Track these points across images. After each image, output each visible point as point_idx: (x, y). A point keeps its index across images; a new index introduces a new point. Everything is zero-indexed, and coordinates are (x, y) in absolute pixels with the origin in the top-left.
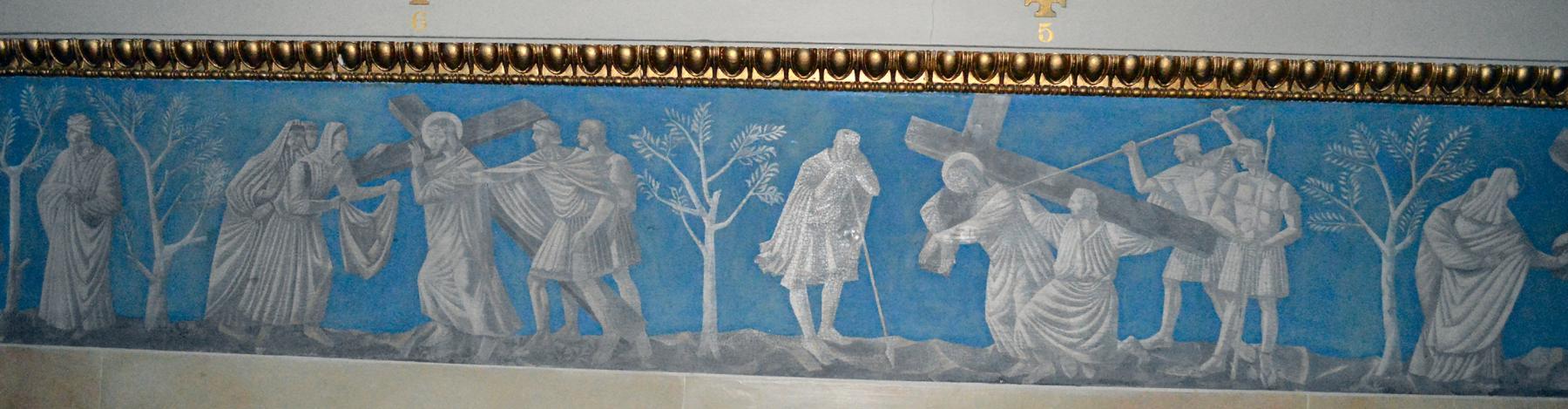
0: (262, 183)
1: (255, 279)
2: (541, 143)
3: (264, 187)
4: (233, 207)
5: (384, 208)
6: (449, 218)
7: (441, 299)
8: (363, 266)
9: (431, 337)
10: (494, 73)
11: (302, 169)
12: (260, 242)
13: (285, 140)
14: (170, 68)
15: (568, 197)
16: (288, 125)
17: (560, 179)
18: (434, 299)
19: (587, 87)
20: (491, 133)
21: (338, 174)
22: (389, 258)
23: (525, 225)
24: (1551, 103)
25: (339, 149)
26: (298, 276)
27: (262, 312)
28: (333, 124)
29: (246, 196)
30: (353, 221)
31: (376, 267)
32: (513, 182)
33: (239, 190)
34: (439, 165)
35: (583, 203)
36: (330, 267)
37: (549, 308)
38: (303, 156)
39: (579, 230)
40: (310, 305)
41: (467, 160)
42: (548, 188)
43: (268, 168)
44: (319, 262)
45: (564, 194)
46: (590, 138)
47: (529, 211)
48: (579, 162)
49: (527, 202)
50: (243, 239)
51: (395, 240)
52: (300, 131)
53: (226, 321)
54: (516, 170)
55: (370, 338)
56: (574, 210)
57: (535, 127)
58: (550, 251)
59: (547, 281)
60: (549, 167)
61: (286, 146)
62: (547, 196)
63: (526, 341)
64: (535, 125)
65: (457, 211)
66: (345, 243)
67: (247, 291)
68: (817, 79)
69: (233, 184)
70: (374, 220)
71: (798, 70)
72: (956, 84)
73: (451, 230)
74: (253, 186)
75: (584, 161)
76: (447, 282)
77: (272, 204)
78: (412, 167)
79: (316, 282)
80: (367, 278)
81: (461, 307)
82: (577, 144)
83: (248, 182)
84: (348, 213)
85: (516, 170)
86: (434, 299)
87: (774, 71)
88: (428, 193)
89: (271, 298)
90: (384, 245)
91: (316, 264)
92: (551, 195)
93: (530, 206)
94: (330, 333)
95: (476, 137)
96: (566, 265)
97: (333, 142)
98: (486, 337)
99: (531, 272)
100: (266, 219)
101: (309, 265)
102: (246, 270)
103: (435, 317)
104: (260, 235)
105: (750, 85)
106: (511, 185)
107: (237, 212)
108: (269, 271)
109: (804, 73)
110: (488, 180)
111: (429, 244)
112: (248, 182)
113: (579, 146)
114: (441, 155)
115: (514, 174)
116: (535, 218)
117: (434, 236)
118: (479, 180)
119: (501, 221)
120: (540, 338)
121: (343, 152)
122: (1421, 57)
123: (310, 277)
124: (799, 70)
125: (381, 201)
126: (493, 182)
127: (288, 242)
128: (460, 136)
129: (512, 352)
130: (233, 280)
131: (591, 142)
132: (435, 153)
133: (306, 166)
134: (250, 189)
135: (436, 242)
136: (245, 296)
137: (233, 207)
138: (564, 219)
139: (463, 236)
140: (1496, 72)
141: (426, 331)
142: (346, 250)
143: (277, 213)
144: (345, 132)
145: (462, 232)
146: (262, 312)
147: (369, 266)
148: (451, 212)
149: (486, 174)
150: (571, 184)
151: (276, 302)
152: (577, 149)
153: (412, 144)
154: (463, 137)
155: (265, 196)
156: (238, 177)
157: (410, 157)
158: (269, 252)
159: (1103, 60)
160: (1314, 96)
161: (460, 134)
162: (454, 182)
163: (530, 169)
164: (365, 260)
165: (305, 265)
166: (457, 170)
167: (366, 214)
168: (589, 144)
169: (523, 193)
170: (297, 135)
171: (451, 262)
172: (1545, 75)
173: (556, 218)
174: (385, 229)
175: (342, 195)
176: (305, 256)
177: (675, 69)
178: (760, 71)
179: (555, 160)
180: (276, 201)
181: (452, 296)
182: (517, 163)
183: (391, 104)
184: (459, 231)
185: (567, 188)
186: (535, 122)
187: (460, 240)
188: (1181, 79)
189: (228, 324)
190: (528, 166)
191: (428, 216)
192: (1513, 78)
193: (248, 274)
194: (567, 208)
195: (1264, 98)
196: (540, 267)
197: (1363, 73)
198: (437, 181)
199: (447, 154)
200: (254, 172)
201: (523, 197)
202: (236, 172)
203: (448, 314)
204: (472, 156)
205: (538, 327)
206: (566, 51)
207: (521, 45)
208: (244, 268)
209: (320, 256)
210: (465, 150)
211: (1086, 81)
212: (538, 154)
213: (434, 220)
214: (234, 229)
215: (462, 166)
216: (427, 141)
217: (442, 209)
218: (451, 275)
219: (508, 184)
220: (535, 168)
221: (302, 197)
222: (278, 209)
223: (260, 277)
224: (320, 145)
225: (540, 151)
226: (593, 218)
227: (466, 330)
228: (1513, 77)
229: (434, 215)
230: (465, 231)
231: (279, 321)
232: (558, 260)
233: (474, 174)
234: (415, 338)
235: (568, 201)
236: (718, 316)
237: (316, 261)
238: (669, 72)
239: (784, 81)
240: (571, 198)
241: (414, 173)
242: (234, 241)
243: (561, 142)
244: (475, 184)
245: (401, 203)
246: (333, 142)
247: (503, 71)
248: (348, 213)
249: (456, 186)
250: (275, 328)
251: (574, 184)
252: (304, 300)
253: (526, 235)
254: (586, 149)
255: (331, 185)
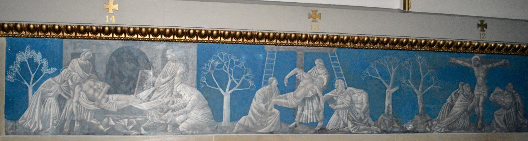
10: (59, 35)
14: (11, 33)
19: (130, 41)
24: (403, 49)
68: (242, 41)
71: (178, 36)
72: (251, 42)
87: (169, 36)
105: (243, 43)
109: (180, 37)
122: (28, 22)
124: (178, 36)
136: (38, 105)
140: (388, 40)
159: (241, 33)
160: (326, 46)
172: (362, 39)
177: (219, 37)
178: (165, 36)
188: (75, 32)
192: (402, 42)
195: (429, 51)
197: (209, 34)
206: (48, 26)
207: (56, 25)
211: (236, 40)
228: (412, 42)
238: (109, 35)
239: (124, 37)
247: (359, 45)
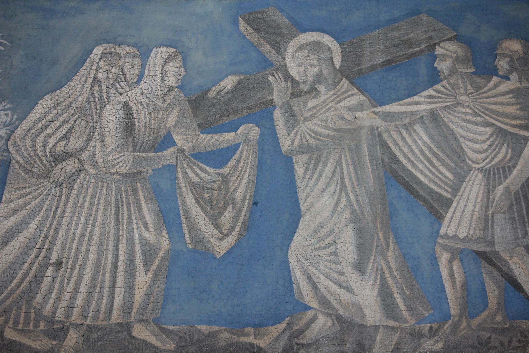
0: (63, 131)
1: (59, 264)
2: (446, 72)
3: (66, 137)
4: (20, 165)
5: (238, 161)
6: (328, 172)
7: (322, 280)
8: (212, 240)
9: (307, 332)
11: (121, 112)
12: (64, 212)
13: (93, 72)
15: (485, 141)
16: (98, 51)
17: (473, 119)
18: (310, 278)
20: (379, 59)
21: (171, 121)
22: (247, 228)
23: (430, 180)
25: (171, 84)
26: (121, 258)
27: (70, 308)
28: (161, 50)
29: (39, 150)
30: (195, 179)
31: (231, 240)
32: (411, 124)
33: (28, 141)
34: (311, 104)
35: (504, 149)
36: (165, 243)
37: (465, 285)
38: (121, 94)
39: (500, 183)
40: (139, 295)
41: (349, 97)
42: (458, 131)
43: (71, 111)
44: (150, 237)
45: (479, 138)
46: (511, 61)
47: (435, 161)
48: (497, 96)
49: (430, 149)
50: (37, 210)
51: (255, 204)
52: (114, 59)
53: (16, 323)
54: (415, 108)
55: (226, 335)
56: (493, 158)
57: (439, 50)
58: (464, 211)
59: (462, 251)
60: (458, 104)
61: (96, 80)
62: (457, 140)
63: (437, 331)
64: (437, 48)
65: (339, 163)
66: (184, 202)
67: (47, 281)
69: (19, 132)
70: (225, 179)
73: (331, 189)
74: (49, 136)
75: (504, 94)
76: (328, 258)
77: (80, 160)
78: (275, 107)
79: (147, 263)
80: (219, 257)
81: (349, 289)
82: (494, 72)
83: (43, 129)
84: (188, 171)
85: (415, 108)
86: (310, 278)
88: (297, 141)
89: (83, 289)
90: (240, 210)
91: (146, 239)
92: (462, 140)
93: (434, 154)
94: (170, 332)
95: (360, 64)
96: (485, 229)
97: (163, 74)
98: (386, 327)
99: (440, 240)
100: (71, 180)
101: (137, 241)
102: (44, 251)
103: (313, 303)
104: (62, 204)
106: (409, 127)
107: (27, 171)
108: (78, 251)
110: (378, 122)
111: (303, 209)
112: (43, 129)
113: (497, 75)
114: (313, 91)
115: (412, 113)
116: (441, 168)
117: (307, 196)
118: (366, 123)
119: (397, 177)
120: (456, 326)
121: (177, 87)
123: (139, 258)
125: (234, 153)
126: (384, 124)
127: (105, 210)
128: (338, 65)
129: (419, 346)
130: (26, 266)
131: (513, 68)
132: (305, 87)
133: (126, 106)
134: (45, 141)
135: (312, 204)
137: (20, 165)
138: (481, 170)
139: (347, 195)
141: (303, 322)
142: (188, 218)
143: (87, 172)
144: (179, 62)
145: (346, 190)
146: (70, 308)
147: (220, 239)
148: (330, 166)
149: (375, 113)
150: (488, 125)
151: (90, 294)
152: (495, 79)
153: (273, 75)
154: (342, 65)
155: (69, 149)
156: (26, 124)
157: (272, 93)
158: (77, 224)
161: (338, 62)
162: (331, 125)
163: (433, 106)
164: (215, 233)
165: (131, 243)
166: (336, 109)
167: (211, 170)
168: (510, 72)
169: (426, 138)
170: (113, 65)
171: (331, 232)
173: (470, 169)
174: (241, 189)
175: (180, 145)
176: (130, 230)
179: (466, 94)
180: (84, 156)
181: (336, 276)
182: (416, 98)
183: (242, 22)
184: (341, 191)
185: (482, 129)
186: (439, 43)
187: (343, 202)
189: (20, 326)
190: (431, 103)
191: (299, 171)
193: (47, 257)
194: (484, 155)
196: (451, 233)
198: (309, 124)
199: (321, 88)
200: (49, 117)
201: (424, 143)
202: (22, 119)
203: (331, 299)
204: (355, 91)
205: (452, 312)
208: (41, 249)
209: (151, 229)
210: (345, 83)
212: (443, 86)
213: (308, 177)
214: (23, 196)
215: (342, 104)
216: (294, 71)
217: (317, 161)
218: (333, 247)
219: (404, 126)
220: (438, 105)
221: (121, 148)
222: (87, 167)
223: (64, 260)
224: (145, 78)
225: (445, 83)
226: (518, 167)
227: (358, 320)
229: (307, 169)
230: (349, 190)
231: (96, 317)
232: (474, 223)
233: (359, 114)
234: (288, 334)
235: (485, 146)
236: (401, 112)
237: (146, 235)
240: (488, 143)
241: (278, 116)
242: (24, 212)
243: (473, 70)
244: (360, 128)
245: (261, 150)
246: (163, 74)
248: (188, 171)
249: (336, 130)
250: (91, 329)
251: (493, 125)
252: (130, 288)
253: (432, 192)
254: (507, 78)
255: (163, 133)
